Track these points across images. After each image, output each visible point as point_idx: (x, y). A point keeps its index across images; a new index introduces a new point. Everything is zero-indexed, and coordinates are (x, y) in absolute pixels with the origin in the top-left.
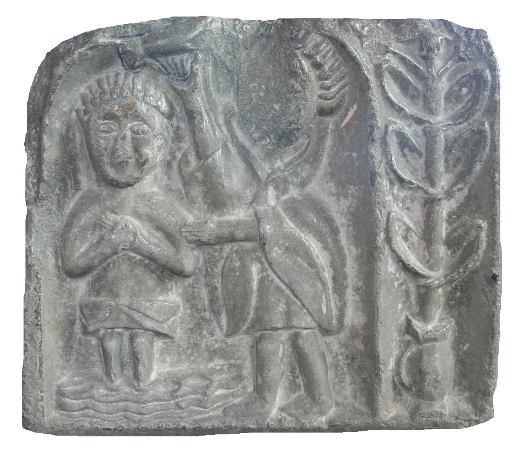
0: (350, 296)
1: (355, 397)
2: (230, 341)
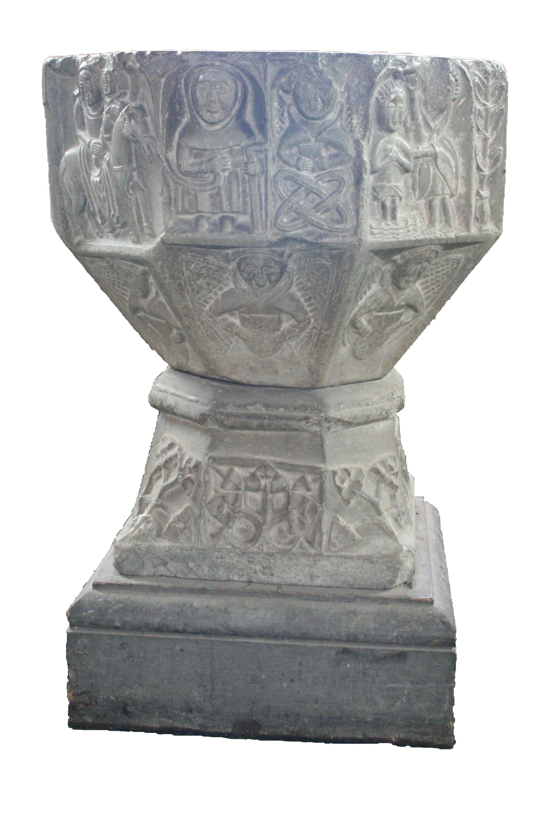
0: (460, 181)
1: (460, 225)
2: (418, 202)
